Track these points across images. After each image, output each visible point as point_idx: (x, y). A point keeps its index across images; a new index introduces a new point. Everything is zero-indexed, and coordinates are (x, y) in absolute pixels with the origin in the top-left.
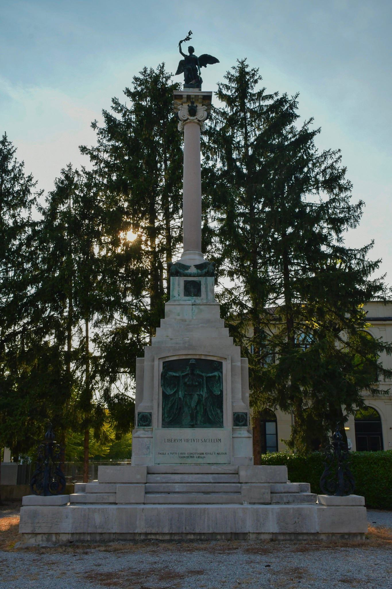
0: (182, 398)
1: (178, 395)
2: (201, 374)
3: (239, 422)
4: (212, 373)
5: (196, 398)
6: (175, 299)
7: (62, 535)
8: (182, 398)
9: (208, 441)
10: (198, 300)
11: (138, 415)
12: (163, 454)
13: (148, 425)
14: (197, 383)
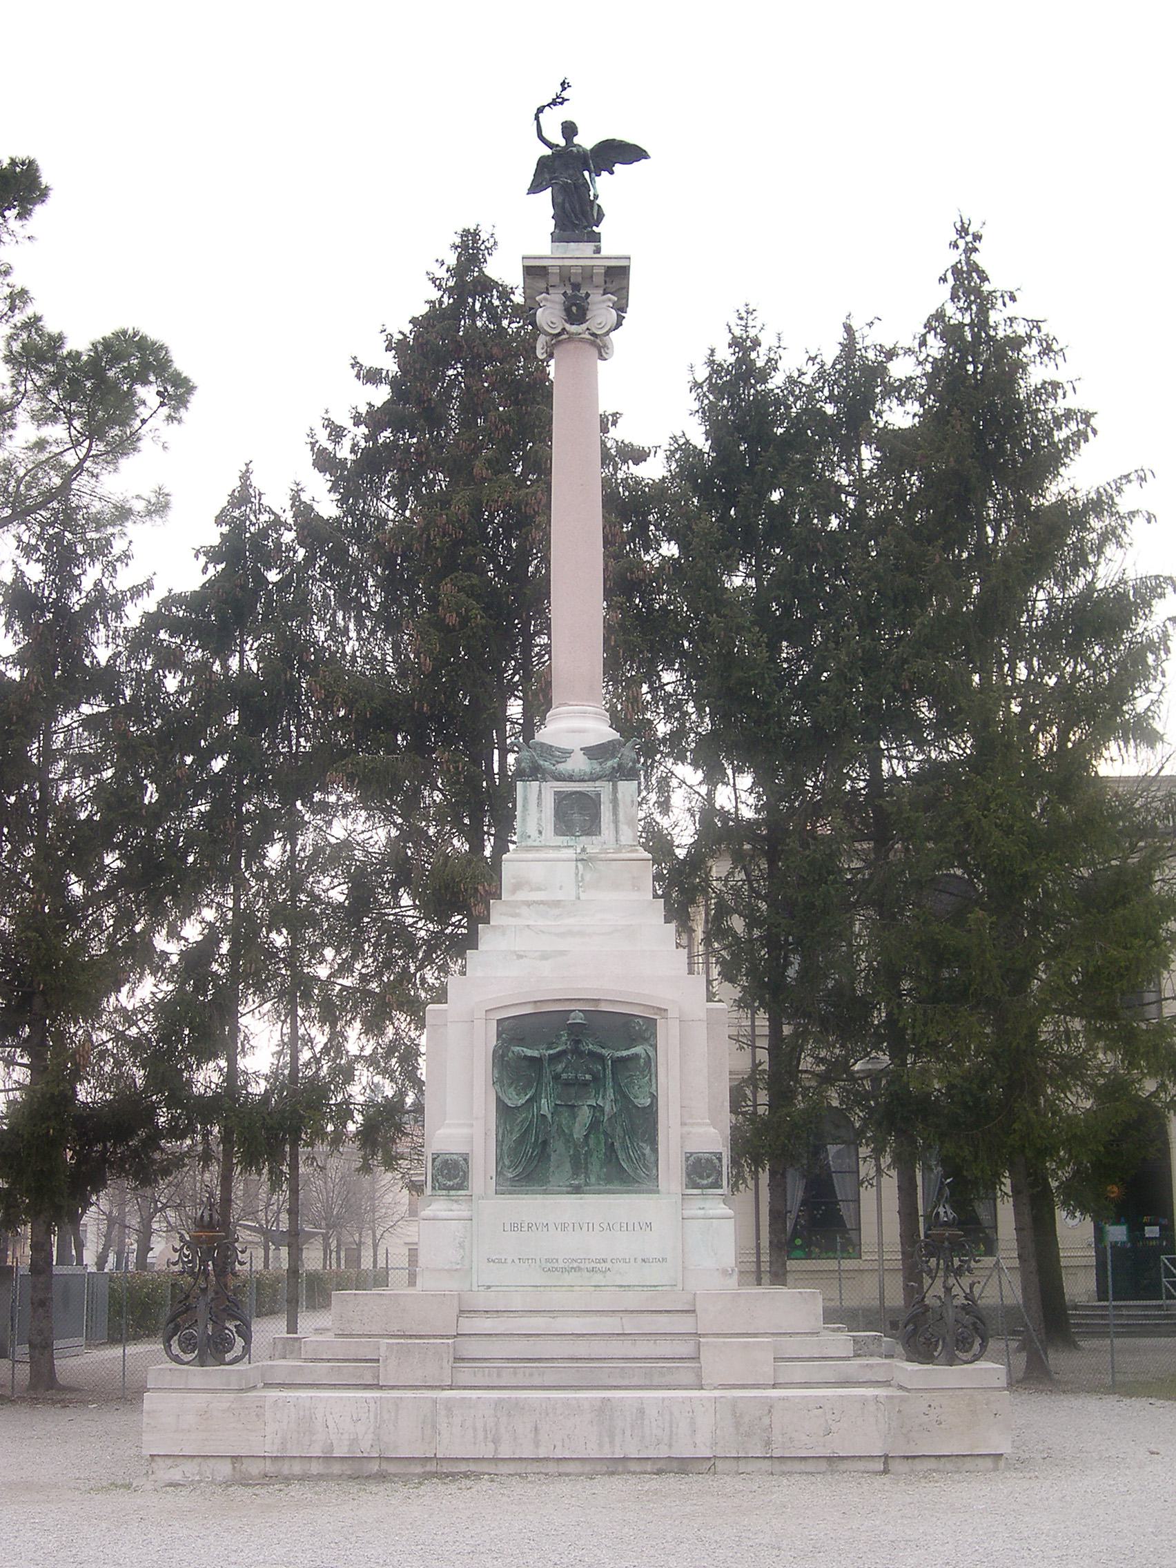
0: (549, 1116)
1: (539, 1108)
2: (600, 1050)
3: (701, 1178)
4: (627, 1049)
5: (585, 1115)
6: (530, 842)
7: (249, 1460)
8: (549, 1116)
9: (617, 1227)
10: (592, 845)
11: (434, 1160)
12: (500, 1261)
13: (460, 1187)
14: (588, 1077)
